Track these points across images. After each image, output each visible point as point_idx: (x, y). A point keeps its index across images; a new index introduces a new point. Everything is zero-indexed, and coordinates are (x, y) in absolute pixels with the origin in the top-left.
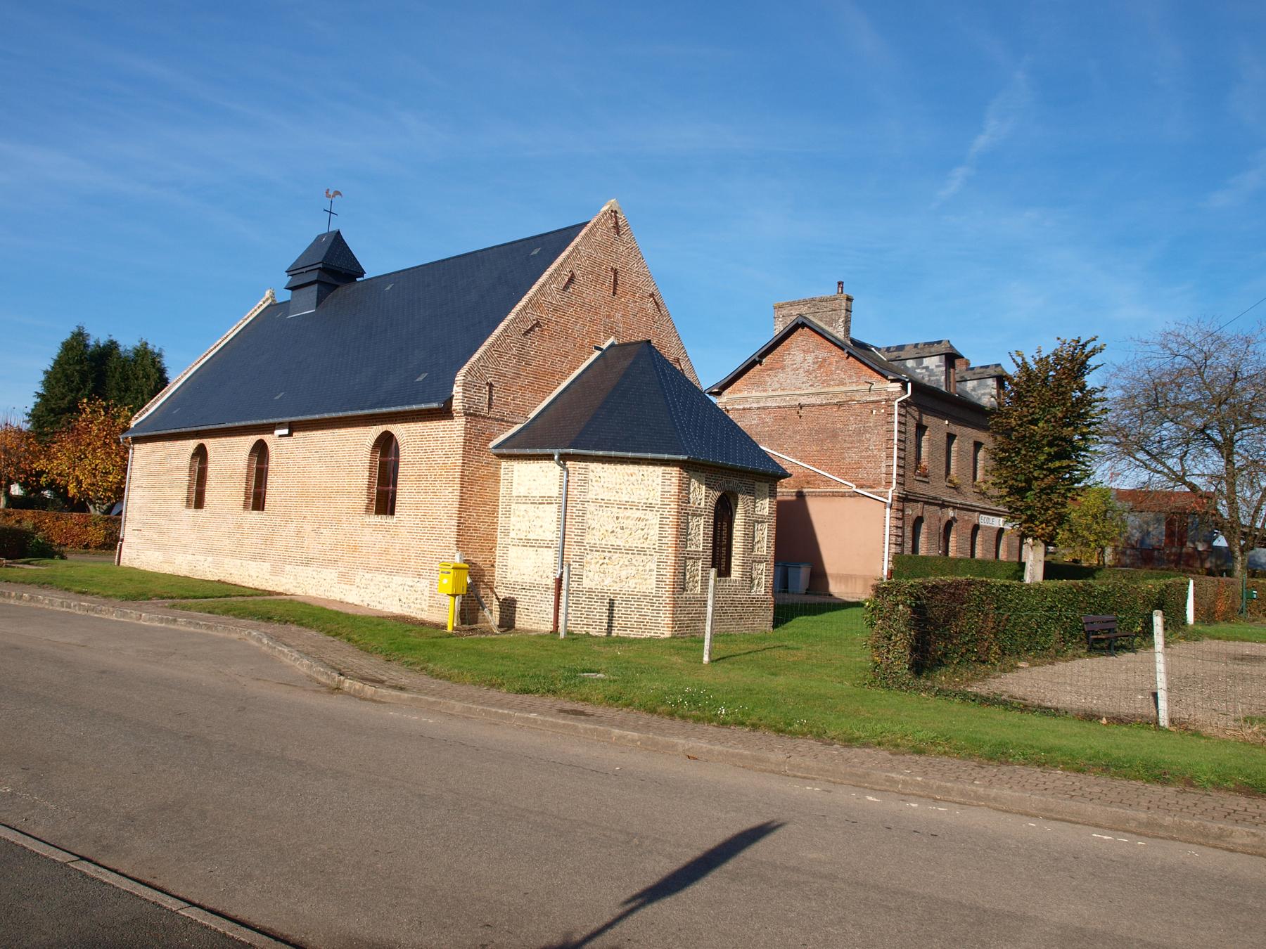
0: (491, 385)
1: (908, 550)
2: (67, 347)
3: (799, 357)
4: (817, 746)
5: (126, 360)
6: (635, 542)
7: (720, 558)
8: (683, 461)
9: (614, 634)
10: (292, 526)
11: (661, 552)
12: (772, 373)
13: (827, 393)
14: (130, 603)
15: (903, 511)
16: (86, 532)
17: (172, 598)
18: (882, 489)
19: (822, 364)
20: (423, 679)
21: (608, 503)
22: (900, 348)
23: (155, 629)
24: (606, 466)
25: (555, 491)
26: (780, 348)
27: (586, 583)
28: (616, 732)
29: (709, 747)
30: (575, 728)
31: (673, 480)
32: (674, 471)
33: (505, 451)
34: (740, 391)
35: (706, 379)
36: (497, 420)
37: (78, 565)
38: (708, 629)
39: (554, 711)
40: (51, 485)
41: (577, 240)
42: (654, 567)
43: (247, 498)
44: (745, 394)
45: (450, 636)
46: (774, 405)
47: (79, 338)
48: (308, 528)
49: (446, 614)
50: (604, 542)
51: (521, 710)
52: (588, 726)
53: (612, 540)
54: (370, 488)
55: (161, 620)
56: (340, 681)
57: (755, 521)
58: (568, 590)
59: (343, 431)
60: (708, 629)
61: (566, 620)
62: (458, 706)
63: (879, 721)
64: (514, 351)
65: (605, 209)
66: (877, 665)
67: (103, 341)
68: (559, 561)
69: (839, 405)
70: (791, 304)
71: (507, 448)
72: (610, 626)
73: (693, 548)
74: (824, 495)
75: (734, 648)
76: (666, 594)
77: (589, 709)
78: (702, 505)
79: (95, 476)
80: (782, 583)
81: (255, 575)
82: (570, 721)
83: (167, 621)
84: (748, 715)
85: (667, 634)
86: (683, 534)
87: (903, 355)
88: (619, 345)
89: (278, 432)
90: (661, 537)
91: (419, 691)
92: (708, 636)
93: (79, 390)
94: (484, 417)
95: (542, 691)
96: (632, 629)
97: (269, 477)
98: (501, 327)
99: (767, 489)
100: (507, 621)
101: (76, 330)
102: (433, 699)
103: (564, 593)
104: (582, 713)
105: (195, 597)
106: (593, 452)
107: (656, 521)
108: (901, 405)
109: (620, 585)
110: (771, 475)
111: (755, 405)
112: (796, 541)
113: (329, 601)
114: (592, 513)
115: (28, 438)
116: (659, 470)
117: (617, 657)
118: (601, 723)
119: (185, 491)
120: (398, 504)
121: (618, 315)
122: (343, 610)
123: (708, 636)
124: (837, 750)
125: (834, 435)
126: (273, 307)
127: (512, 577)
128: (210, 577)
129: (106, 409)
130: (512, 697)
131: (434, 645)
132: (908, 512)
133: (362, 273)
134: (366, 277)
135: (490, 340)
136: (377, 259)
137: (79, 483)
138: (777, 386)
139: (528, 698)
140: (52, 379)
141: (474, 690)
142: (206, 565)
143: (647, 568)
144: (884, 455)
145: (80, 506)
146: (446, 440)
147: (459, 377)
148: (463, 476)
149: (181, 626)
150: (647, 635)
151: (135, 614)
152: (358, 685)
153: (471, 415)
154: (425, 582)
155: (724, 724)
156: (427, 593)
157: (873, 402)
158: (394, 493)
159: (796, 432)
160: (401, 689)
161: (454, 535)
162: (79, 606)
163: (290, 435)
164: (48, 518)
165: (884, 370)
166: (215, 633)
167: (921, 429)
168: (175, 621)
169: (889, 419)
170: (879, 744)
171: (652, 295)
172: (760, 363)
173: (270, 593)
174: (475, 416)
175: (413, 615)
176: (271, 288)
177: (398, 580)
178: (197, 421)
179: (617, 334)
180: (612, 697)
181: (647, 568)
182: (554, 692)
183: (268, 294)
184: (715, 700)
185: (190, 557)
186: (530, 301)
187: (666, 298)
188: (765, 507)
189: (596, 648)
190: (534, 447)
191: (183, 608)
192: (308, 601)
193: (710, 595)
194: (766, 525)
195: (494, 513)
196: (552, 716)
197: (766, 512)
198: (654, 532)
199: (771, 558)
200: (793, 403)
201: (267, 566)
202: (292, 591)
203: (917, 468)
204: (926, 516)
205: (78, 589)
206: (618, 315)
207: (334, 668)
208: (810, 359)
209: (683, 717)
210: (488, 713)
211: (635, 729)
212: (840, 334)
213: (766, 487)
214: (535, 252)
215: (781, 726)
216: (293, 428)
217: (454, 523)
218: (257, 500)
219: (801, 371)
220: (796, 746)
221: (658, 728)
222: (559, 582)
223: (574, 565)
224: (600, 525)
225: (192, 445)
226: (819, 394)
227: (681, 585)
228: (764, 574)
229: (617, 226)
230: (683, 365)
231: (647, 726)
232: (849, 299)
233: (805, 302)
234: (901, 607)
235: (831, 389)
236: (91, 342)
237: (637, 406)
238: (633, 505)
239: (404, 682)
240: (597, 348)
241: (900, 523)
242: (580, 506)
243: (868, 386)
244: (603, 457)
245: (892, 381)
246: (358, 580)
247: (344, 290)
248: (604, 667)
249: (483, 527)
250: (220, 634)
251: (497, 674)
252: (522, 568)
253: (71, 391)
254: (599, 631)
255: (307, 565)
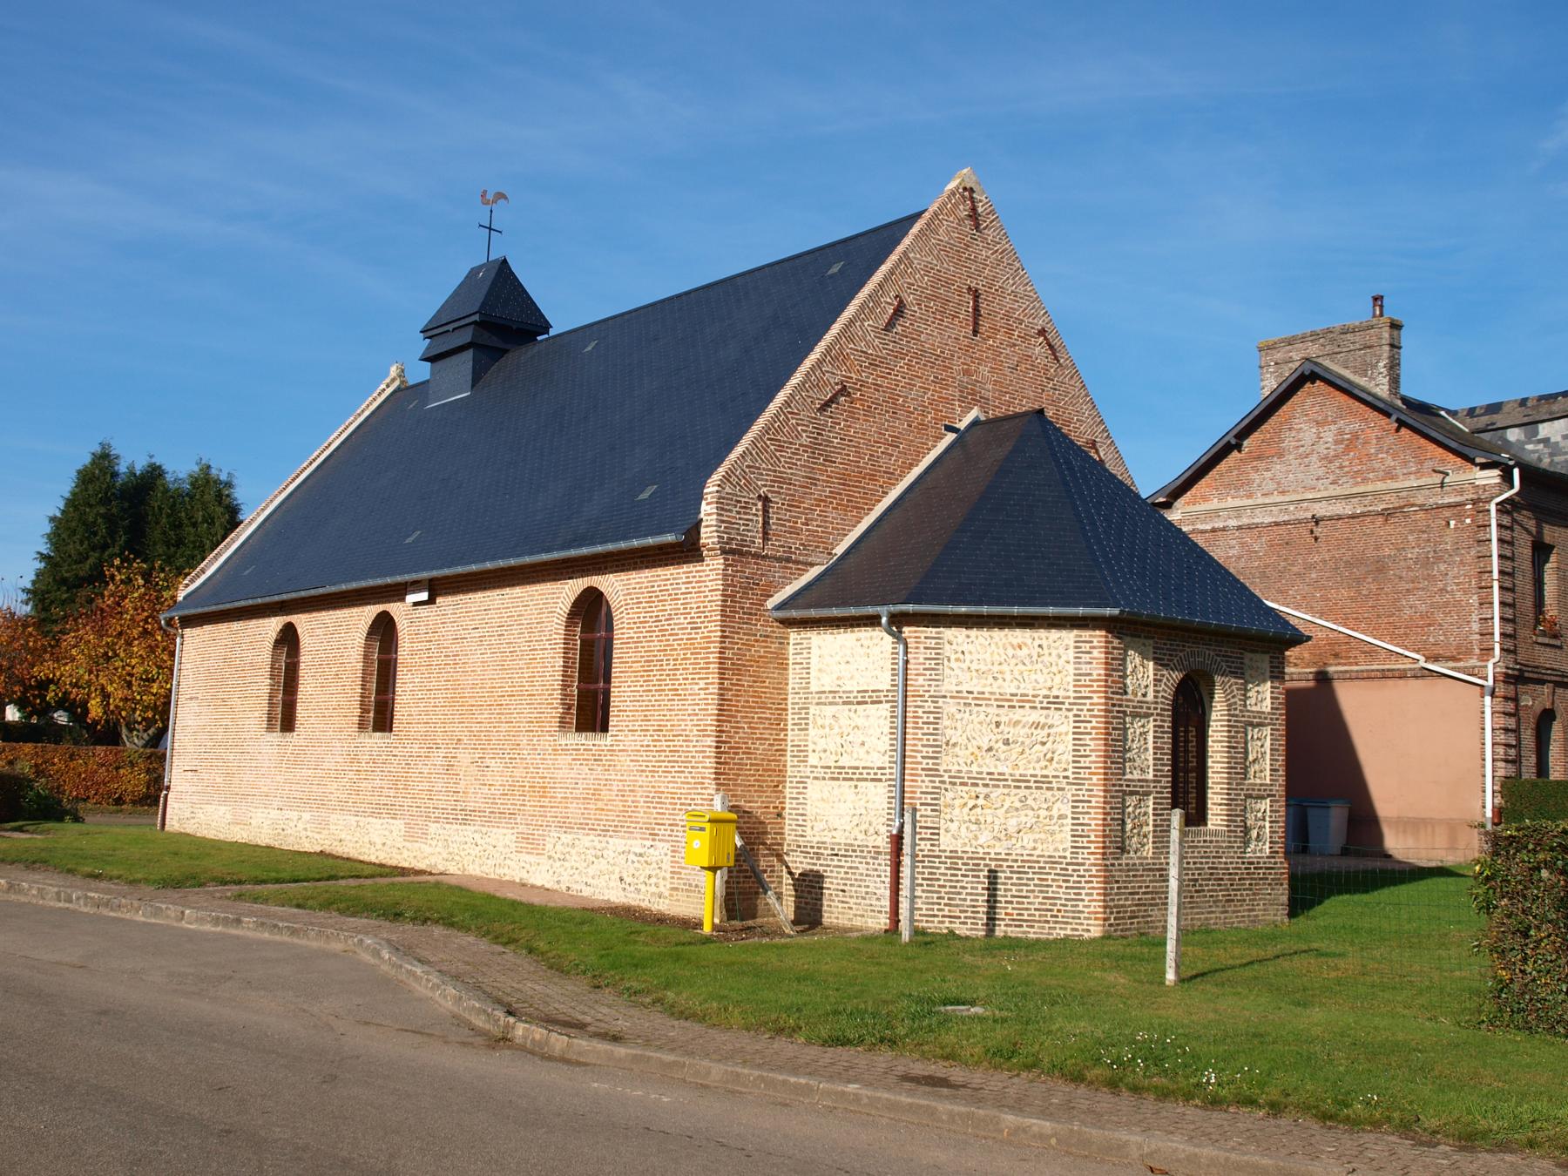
0: (766, 500)
1: (1529, 772)
2: (86, 478)
3: (1308, 433)
4: (1405, 1148)
5: (179, 494)
6: (1031, 767)
7: (1186, 787)
8: (1112, 619)
9: (999, 932)
10: (438, 758)
11: (1078, 782)
12: (1261, 465)
13: (1363, 495)
14: (169, 892)
15: (1516, 700)
16: (117, 778)
17: (240, 882)
18: (1474, 662)
19: (1350, 443)
20: (655, 1021)
21: (980, 699)
22: (1494, 408)
23: (204, 936)
24: (974, 632)
25: (884, 681)
26: (1273, 420)
27: (946, 842)
28: (1010, 1119)
29: (1190, 1149)
30: (932, 1113)
31: (1096, 653)
32: (1097, 637)
33: (794, 614)
34: (1205, 499)
35: (1148, 484)
36: (779, 560)
37: (100, 832)
38: (1172, 921)
39: (892, 1079)
40: (64, 703)
41: (907, 241)
42: (1067, 810)
43: (364, 711)
44: (1214, 504)
45: (707, 940)
46: (1268, 520)
47: (103, 461)
48: (464, 758)
49: (699, 900)
50: (975, 768)
51: (831, 1078)
52: (956, 1108)
53: (989, 765)
54: (565, 686)
55: (216, 921)
56: (507, 1025)
57: (1246, 727)
58: (914, 856)
59: (517, 591)
60: (1172, 921)
61: (912, 909)
62: (717, 1071)
63: (1523, 1097)
64: (805, 440)
65: (952, 185)
66: (1503, 986)
67: (140, 466)
68: (896, 804)
69: (1387, 514)
70: (1290, 342)
71: (797, 608)
72: (991, 919)
73: (1136, 775)
74: (1368, 677)
75: (1221, 956)
76: (1091, 859)
77: (957, 1074)
78: (1150, 697)
79: (130, 685)
80: (1299, 836)
81: (379, 841)
82: (921, 1099)
83: (226, 922)
84: (1262, 1085)
85: (1096, 932)
86: (1117, 750)
87: (1499, 419)
88: (989, 422)
89: (411, 598)
90: (1078, 755)
91: (648, 1043)
92: (1172, 934)
93: (104, 547)
94: (756, 556)
95: (869, 1040)
96: (1031, 923)
97: (399, 675)
98: (781, 397)
99: (1266, 666)
100: (809, 912)
101: (98, 449)
102: (670, 1058)
103: (906, 860)
104: (943, 1082)
105: (278, 881)
106: (950, 609)
107: (1068, 727)
108: (1503, 508)
109: (1005, 844)
110: (1269, 642)
111: (1233, 523)
112: (1321, 761)
113: (501, 883)
114: (951, 717)
115: (25, 626)
116: (1069, 636)
117: (1005, 975)
118: (980, 1101)
119: (265, 703)
120: (613, 712)
121: (984, 370)
122: (524, 897)
123: (1172, 934)
124: (1446, 1156)
125: (1380, 568)
126: (405, 394)
127: (814, 835)
128: (308, 848)
129: (147, 576)
130: (814, 1051)
131: (678, 958)
132: (1526, 701)
133: (546, 327)
134: (552, 332)
135: (761, 421)
136: (572, 296)
137: (106, 696)
138: (1271, 486)
139: (844, 1054)
140: (65, 529)
141: (745, 1041)
142: (301, 826)
143: (1055, 813)
144: (1474, 600)
145: (108, 735)
146: (693, 600)
147: (711, 488)
148: (722, 659)
149: (249, 930)
150: (1060, 933)
151: (173, 911)
152: (539, 1033)
153: (733, 552)
154: (663, 847)
155: (1215, 1103)
156: (666, 866)
157: (1449, 506)
158: (607, 694)
159: (1310, 567)
160: (616, 1039)
161: (710, 763)
162: (83, 899)
163: (431, 601)
164: (56, 756)
165: (1465, 449)
166: (304, 942)
167: (1541, 551)
168: (238, 921)
169: (1481, 535)
170: (1531, 1144)
171: (1042, 332)
172: (1238, 447)
173: (403, 872)
174: (741, 553)
175: (644, 905)
176: (399, 362)
177: (616, 843)
178: (281, 588)
179: (983, 402)
180: (998, 1052)
181: (1055, 813)
182: (893, 1042)
183: (393, 371)
184: (1195, 1057)
185: (275, 814)
186: (828, 350)
187: (1074, 349)
188: (1264, 697)
189: (968, 958)
190: (845, 603)
191: (255, 900)
192: (464, 883)
193: (1174, 859)
194: (1267, 731)
195: (779, 722)
196: (889, 1089)
197: (1267, 706)
198: (1065, 748)
199: (1279, 789)
200: (1302, 515)
201: (398, 825)
202: (441, 868)
203: (1537, 622)
204: (1560, 708)
205: (88, 869)
206: (984, 370)
207: (499, 1002)
208: (1329, 435)
209: (1136, 1089)
210: (771, 1084)
211: (1045, 1113)
212: (1381, 388)
213: (1264, 662)
214: (835, 269)
215: (1328, 1106)
216: (437, 589)
217: (711, 741)
218: (380, 716)
219: (1314, 458)
220: (1362, 1149)
221: (1090, 1111)
222: (897, 840)
223: (923, 810)
224: (967, 738)
225: (274, 625)
226: (1348, 497)
227: (1116, 843)
228: (1267, 818)
229: (974, 215)
230: (1103, 452)
231: (1068, 1107)
232: (1395, 326)
233: (1315, 336)
234: (1545, 874)
235: (1370, 487)
236: (122, 468)
237: (1022, 526)
238: (1024, 701)
239: (622, 1025)
240: (950, 429)
241: (1512, 723)
242: (929, 706)
243: (1437, 478)
244: (990, 617)
245: (1484, 467)
246: (549, 846)
247: (521, 356)
248: (982, 994)
249: (761, 748)
250: (312, 943)
251: (788, 1009)
252: (832, 820)
253: (94, 549)
254: (970, 927)
255: (465, 822)
